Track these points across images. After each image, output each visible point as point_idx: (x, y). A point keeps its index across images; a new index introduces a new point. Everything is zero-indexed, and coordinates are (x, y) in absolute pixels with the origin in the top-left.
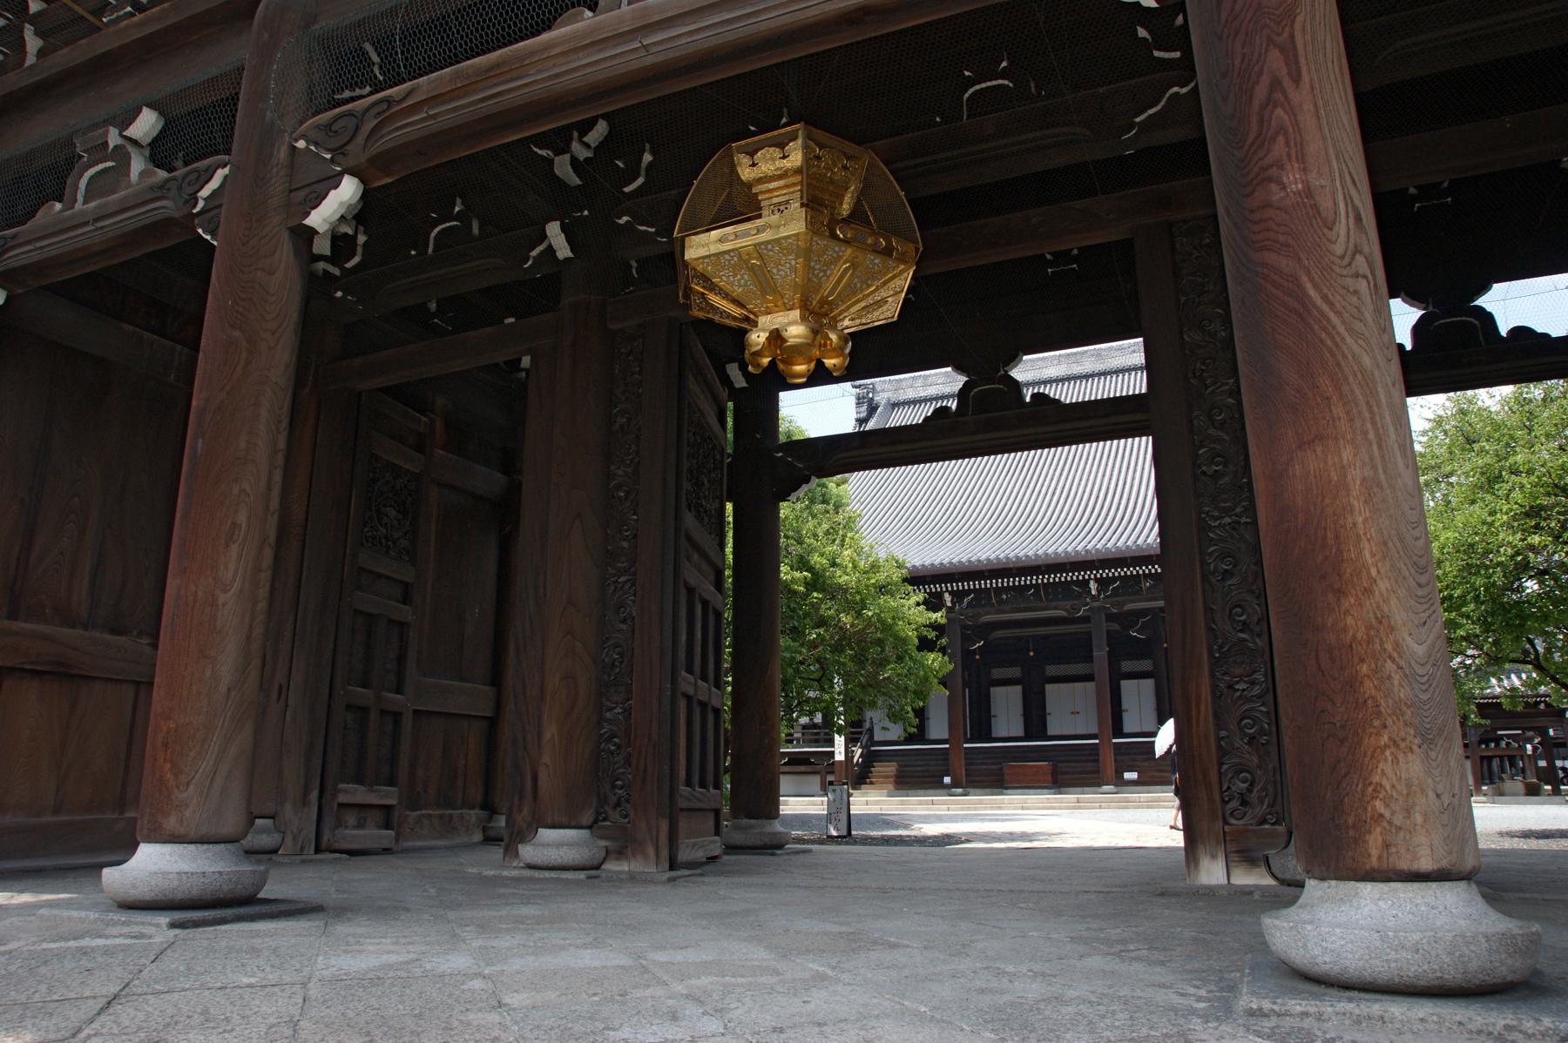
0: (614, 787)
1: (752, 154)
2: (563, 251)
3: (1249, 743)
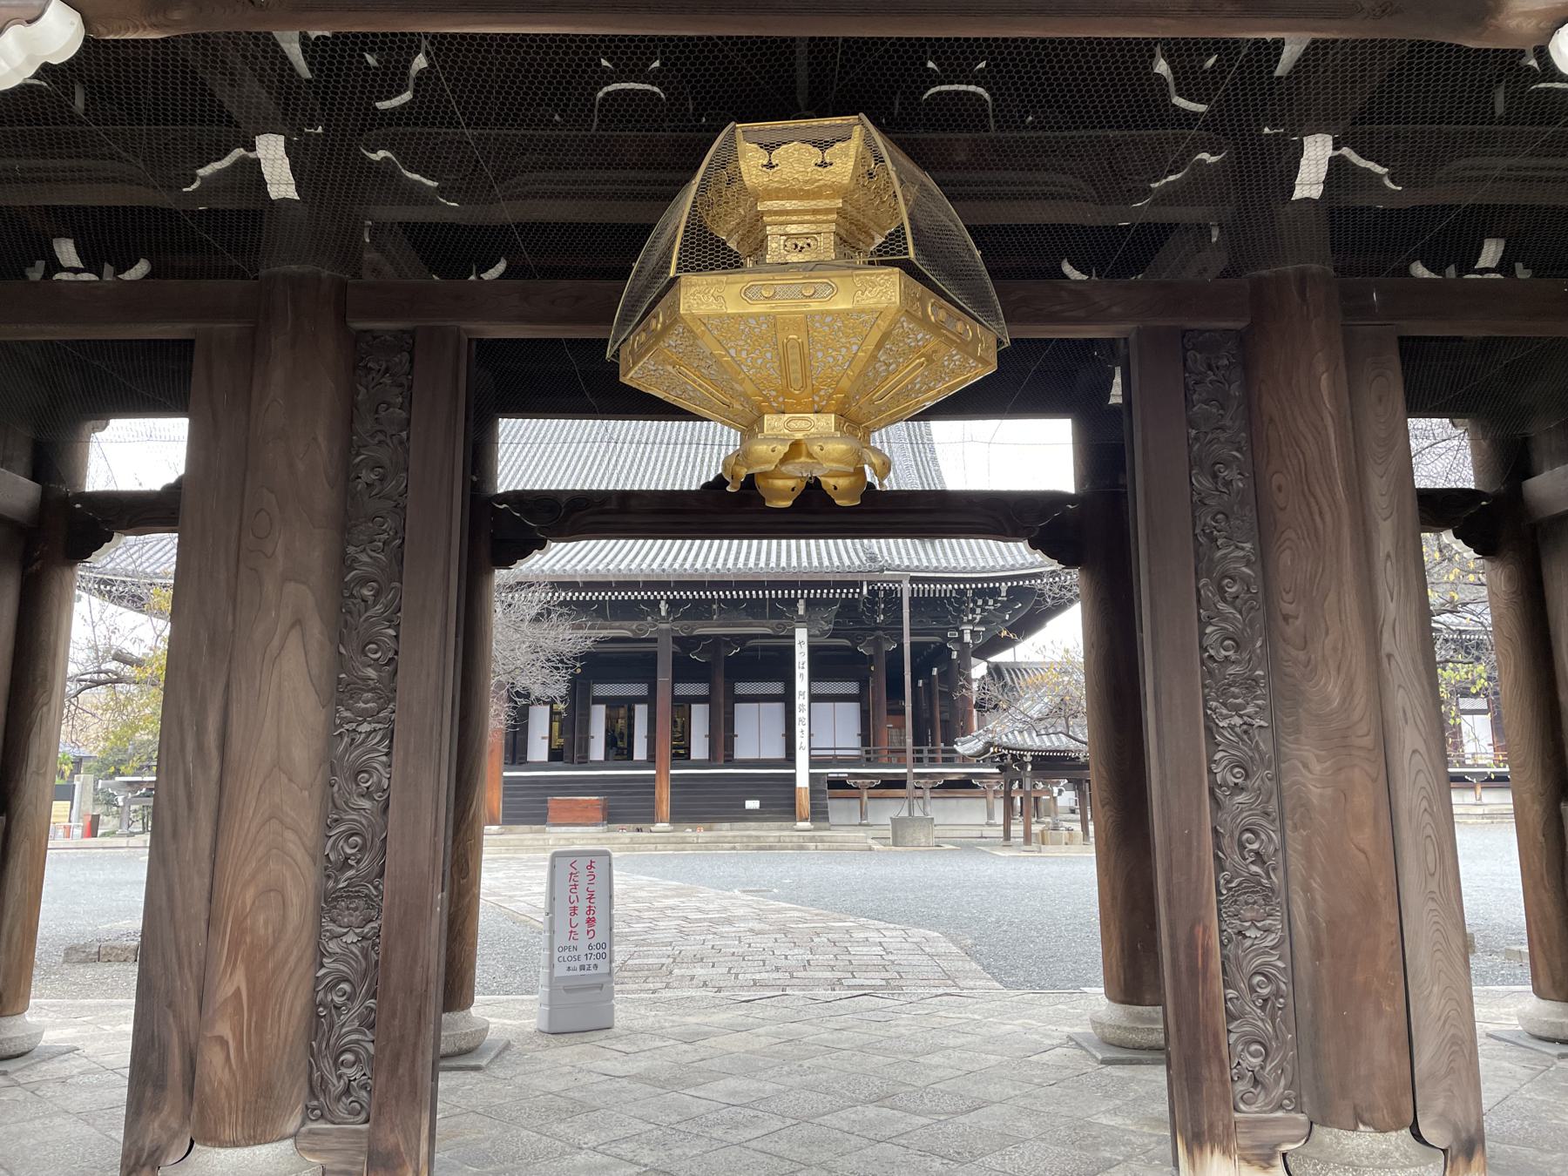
0: (337, 1064)
1: (770, 148)
2: (280, 181)
3: (1262, 1008)
